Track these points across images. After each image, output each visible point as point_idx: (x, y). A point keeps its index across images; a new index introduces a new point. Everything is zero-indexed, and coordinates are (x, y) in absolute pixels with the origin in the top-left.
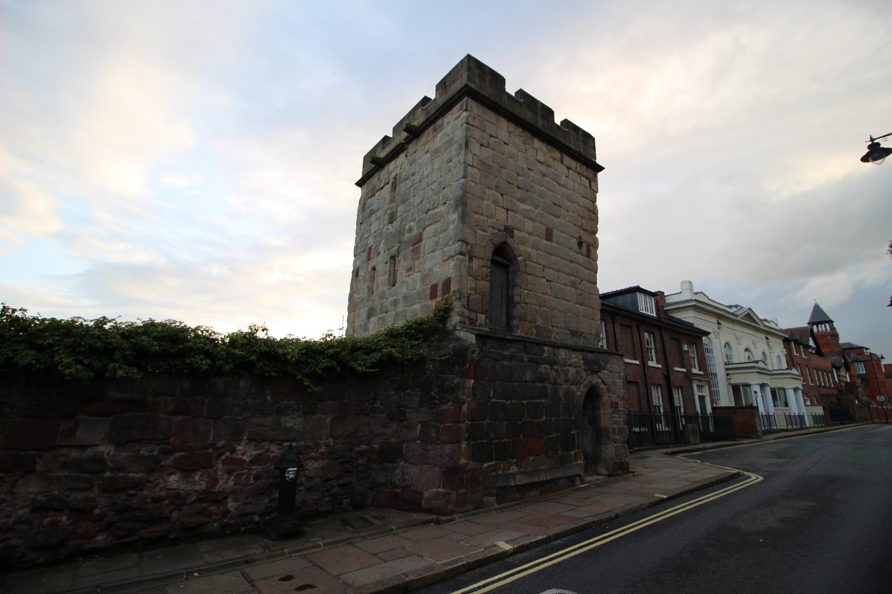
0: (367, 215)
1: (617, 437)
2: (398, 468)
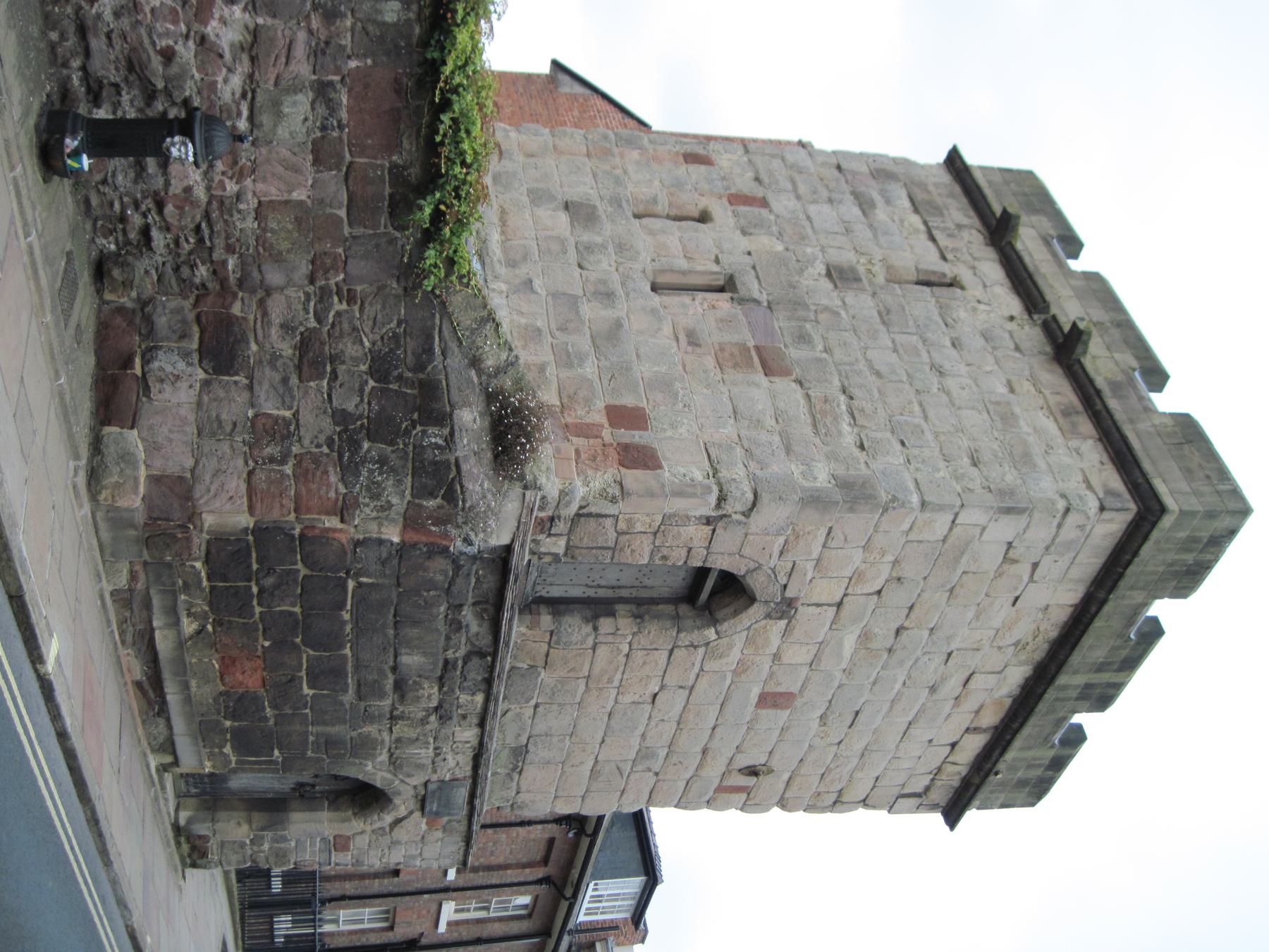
0: (862, 189)
1: (266, 846)
2: (189, 364)
